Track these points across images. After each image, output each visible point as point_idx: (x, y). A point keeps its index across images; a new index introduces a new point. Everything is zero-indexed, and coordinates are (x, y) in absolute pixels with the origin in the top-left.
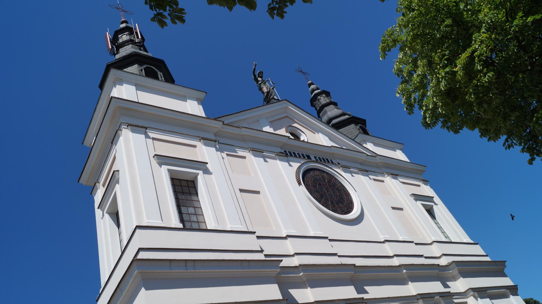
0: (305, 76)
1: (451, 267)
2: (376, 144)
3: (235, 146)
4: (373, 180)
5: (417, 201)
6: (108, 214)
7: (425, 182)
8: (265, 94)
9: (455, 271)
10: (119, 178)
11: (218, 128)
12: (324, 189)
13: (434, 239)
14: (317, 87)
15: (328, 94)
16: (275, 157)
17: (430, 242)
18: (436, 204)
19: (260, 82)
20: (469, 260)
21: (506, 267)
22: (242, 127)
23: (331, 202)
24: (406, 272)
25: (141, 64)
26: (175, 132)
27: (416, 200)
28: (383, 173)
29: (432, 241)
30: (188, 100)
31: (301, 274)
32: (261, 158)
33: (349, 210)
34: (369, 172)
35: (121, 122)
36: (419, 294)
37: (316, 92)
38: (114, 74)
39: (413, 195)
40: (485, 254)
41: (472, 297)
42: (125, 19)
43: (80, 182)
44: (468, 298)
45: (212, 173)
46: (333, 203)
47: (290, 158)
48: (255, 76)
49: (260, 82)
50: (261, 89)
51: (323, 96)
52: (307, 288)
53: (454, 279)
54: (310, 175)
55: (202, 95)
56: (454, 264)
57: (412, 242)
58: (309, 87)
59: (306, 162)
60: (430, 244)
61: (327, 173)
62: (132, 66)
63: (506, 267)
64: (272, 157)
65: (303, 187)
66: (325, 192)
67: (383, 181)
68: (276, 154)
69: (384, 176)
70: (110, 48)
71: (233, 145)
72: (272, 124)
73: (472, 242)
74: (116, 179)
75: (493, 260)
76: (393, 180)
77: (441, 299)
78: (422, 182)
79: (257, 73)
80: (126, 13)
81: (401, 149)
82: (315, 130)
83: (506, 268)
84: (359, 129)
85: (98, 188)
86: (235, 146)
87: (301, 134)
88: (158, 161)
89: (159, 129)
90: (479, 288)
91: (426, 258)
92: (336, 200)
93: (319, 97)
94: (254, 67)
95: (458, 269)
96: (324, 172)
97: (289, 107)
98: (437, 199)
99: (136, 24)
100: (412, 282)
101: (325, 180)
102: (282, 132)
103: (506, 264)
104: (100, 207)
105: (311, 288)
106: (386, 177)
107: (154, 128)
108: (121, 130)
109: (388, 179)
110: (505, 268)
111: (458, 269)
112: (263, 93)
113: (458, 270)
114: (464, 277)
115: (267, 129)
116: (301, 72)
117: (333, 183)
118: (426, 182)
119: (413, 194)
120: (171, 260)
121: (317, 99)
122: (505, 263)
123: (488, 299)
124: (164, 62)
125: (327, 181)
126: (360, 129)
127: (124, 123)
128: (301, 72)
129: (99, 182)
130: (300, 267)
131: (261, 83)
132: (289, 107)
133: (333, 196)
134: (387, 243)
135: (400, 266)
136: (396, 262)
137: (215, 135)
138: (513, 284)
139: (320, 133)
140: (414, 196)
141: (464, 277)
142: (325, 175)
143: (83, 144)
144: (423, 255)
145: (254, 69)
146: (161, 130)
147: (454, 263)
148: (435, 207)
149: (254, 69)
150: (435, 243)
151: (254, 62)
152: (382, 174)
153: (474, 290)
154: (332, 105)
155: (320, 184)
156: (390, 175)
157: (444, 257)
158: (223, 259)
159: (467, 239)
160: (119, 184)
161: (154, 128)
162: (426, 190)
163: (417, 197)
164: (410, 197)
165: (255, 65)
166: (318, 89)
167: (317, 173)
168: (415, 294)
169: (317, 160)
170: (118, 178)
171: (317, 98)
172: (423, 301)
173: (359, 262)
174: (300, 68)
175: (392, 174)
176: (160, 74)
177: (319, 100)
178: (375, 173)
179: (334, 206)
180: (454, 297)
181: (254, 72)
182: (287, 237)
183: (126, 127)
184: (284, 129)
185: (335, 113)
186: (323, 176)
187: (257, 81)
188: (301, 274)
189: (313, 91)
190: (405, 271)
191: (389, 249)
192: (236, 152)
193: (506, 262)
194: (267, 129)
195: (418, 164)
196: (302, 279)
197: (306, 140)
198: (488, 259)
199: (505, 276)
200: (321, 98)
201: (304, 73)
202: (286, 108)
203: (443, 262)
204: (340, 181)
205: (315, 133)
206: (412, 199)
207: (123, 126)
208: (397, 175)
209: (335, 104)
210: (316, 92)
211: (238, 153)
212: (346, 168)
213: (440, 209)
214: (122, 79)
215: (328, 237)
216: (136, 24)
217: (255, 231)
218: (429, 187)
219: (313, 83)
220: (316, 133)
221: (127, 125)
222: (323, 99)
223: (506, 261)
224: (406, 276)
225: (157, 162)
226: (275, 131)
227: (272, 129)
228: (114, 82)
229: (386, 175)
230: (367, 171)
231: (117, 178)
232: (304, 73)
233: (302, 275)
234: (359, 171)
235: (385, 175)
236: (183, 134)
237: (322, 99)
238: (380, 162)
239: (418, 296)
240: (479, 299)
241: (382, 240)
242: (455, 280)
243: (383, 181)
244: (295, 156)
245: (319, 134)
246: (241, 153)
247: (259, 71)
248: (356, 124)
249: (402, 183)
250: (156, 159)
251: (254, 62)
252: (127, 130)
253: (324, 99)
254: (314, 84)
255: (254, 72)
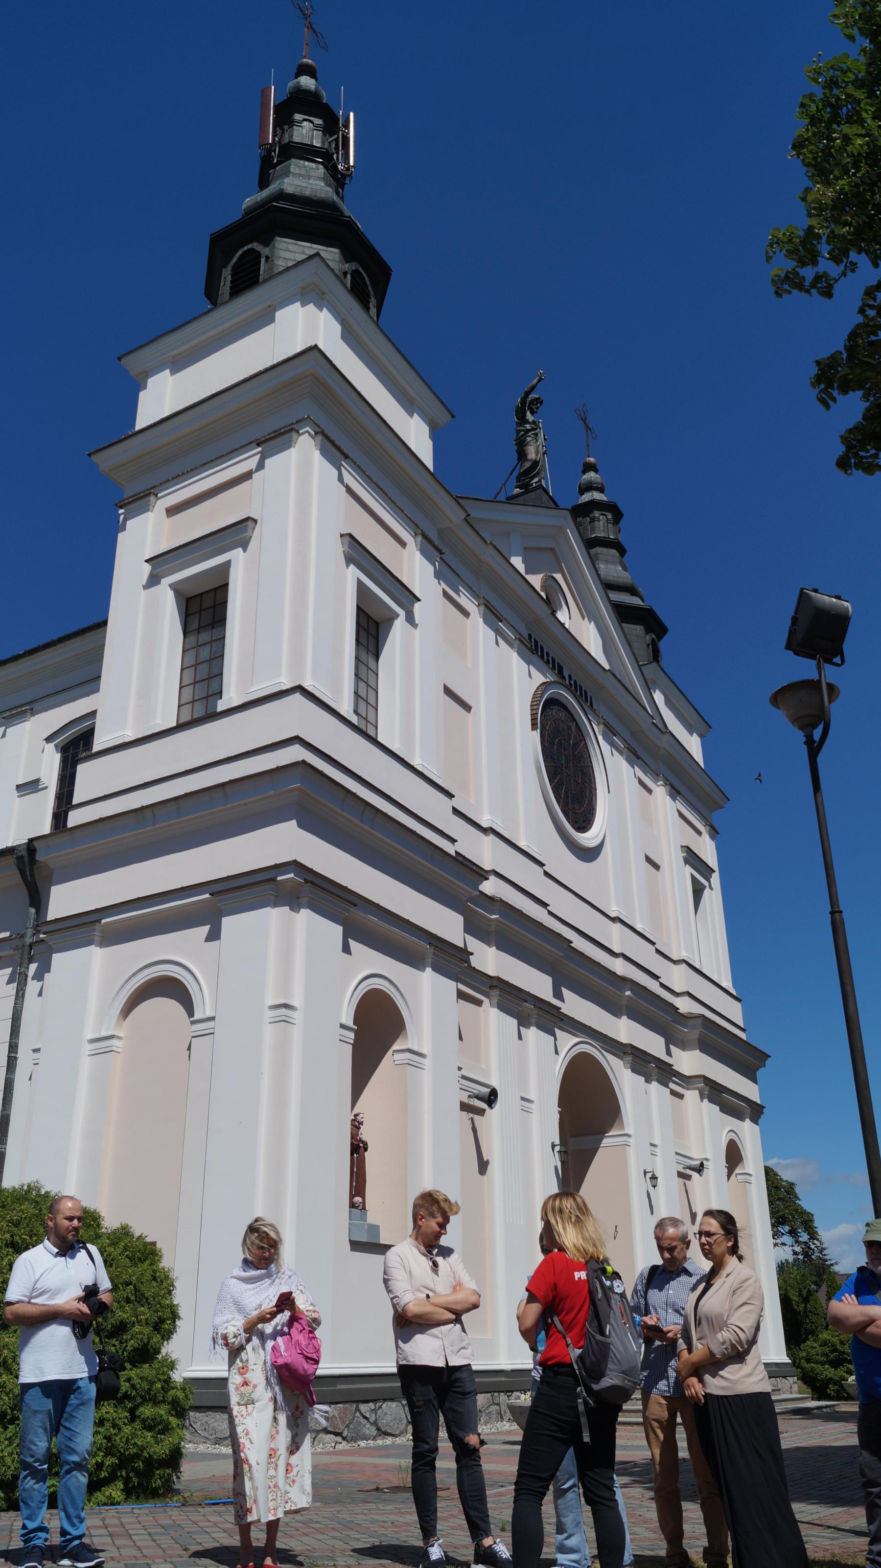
0: (587, 435)
1: (691, 1022)
2: (668, 703)
3: (461, 578)
4: (637, 780)
5: (687, 866)
6: (172, 592)
7: (713, 831)
8: (527, 465)
9: (693, 1033)
10: (251, 537)
11: (452, 522)
12: (563, 757)
13: (684, 955)
14: (602, 484)
15: (618, 515)
16: (512, 641)
17: (675, 958)
18: (711, 888)
19: (528, 426)
20: (226, 875)
21: (764, 1066)
22: (491, 543)
23: (566, 793)
24: (628, 996)
25: (347, 256)
26: (384, 492)
27: (687, 861)
28: (658, 775)
29: (682, 958)
30: (415, 415)
31: (493, 917)
32: (493, 630)
33: (584, 824)
34: (640, 760)
35: (309, 417)
36: (631, 1046)
37: (597, 496)
38: (316, 273)
39: (686, 849)
40: (742, 1025)
41: (697, 1092)
42: (314, 63)
43: (96, 458)
44: (688, 1089)
45: (417, 625)
46: (567, 797)
47: (535, 658)
48: (523, 402)
49: (528, 426)
50: (521, 445)
51: (606, 516)
52: (489, 945)
53: (684, 1046)
54: (552, 714)
55: (443, 417)
56: (700, 1021)
57: (653, 943)
58: (584, 472)
59: (560, 683)
60: (675, 962)
61: (577, 724)
62: (327, 246)
63: (764, 1066)
64: (508, 637)
65: (536, 735)
66: (562, 764)
67: (650, 791)
68: (518, 636)
69: (656, 781)
70: (270, 142)
71: (458, 575)
72: (528, 554)
73: (734, 992)
74: (242, 536)
75: (748, 1041)
76: (668, 798)
77: (656, 1071)
78: (708, 828)
79: (533, 396)
80: (315, 37)
81: (701, 736)
82: (589, 612)
83: (763, 1068)
84: (648, 645)
85: (151, 508)
86: (461, 578)
87: (561, 606)
88: (349, 550)
89: (362, 470)
90: (714, 1082)
91: (662, 985)
92: (573, 792)
93: (597, 514)
94: (535, 381)
95: (701, 1032)
96: (574, 720)
97: (568, 530)
98: (715, 878)
99: (352, 115)
100: (628, 1017)
101: (570, 738)
102: (536, 580)
103: (768, 1062)
104: (154, 562)
105: (498, 948)
106: (658, 786)
107: (355, 463)
108: (298, 432)
109: (660, 791)
110: (761, 1067)
111: (701, 1032)
112: (522, 455)
113: (700, 1035)
114: (702, 1051)
115: (517, 562)
116: (584, 421)
117: (579, 752)
118: (714, 832)
119: (688, 847)
120: (367, 804)
121: (591, 515)
122: (766, 1059)
123: (717, 1108)
124: (390, 275)
125: (573, 742)
126: (650, 646)
127: (313, 421)
128: (584, 421)
129: (156, 495)
130: (498, 903)
131: (529, 431)
132: (568, 530)
133: (572, 780)
134: (619, 925)
135: (624, 979)
136: (619, 967)
137: (441, 532)
138: (759, 1102)
139: (592, 622)
140: (687, 852)
141: (701, 1051)
142: (573, 726)
143: (119, 359)
144: (660, 978)
145: (533, 388)
146: (365, 473)
147: (702, 1018)
148: (707, 892)
149: (533, 388)
150: (684, 965)
151: (542, 372)
152: (656, 775)
153: (707, 1081)
154: (615, 551)
155: (560, 744)
156: (668, 787)
157: (687, 998)
158: (414, 830)
159: (727, 983)
160: (245, 550)
161: (355, 463)
162: (708, 850)
163: (692, 858)
164: (679, 849)
165: (540, 380)
166: (601, 490)
167: (562, 714)
168: (624, 1042)
169: (571, 685)
170: (248, 537)
171: (592, 512)
172: (633, 1060)
173: (579, 944)
174: (585, 409)
175: (672, 786)
176: (373, 301)
177: (593, 520)
178: (647, 768)
179: (568, 804)
180: (673, 1078)
181: (527, 394)
182: (490, 831)
183: (313, 433)
184: (542, 575)
185: (615, 574)
186: (569, 727)
187: (523, 420)
188: (493, 917)
189: (589, 487)
190: (628, 993)
191: (616, 937)
192: (457, 592)
193: (769, 1059)
194: (517, 562)
195: (726, 794)
196: (489, 926)
197: (567, 626)
198: (742, 1035)
199: (754, 1080)
200: (601, 517)
201: (588, 428)
202: (560, 527)
203: (684, 1005)
204: (592, 753)
205: (583, 618)
206: (681, 855)
207: (308, 428)
208: (679, 793)
209: (622, 552)
210: (597, 496)
211: (459, 595)
212: (610, 731)
213: (713, 898)
214: (323, 294)
215: (544, 865)
216: (352, 115)
217: (453, 794)
218: (713, 844)
219: (598, 467)
220: (586, 618)
221: (318, 430)
222: (604, 524)
223: (770, 1057)
224: (624, 1003)
225: (344, 551)
226: (526, 573)
227: (523, 566)
228: (303, 288)
229: (661, 783)
230: (638, 757)
231: (246, 536)
232: (588, 428)
233: (494, 919)
234: (626, 750)
235: (658, 781)
236: (395, 504)
237: (601, 523)
238: (665, 750)
239: (630, 1048)
240: (706, 1101)
241: (613, 915)
242: (684, 1049)
243: (650, 791)
244: (542, 657)
245: (590, 623)
246: (465, 600)
247: (537, 396)
248: (648, 631)
249: (677, 813)
250: (346, 546)
251: (542, 372)
252: (312, 441)
253: (606, 525)
254: (596, 471)
255: (527, 394)
